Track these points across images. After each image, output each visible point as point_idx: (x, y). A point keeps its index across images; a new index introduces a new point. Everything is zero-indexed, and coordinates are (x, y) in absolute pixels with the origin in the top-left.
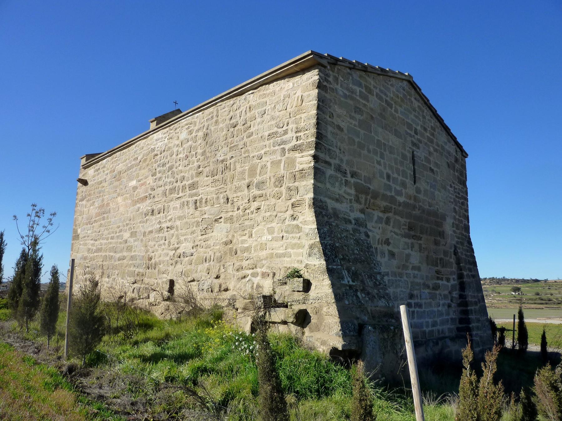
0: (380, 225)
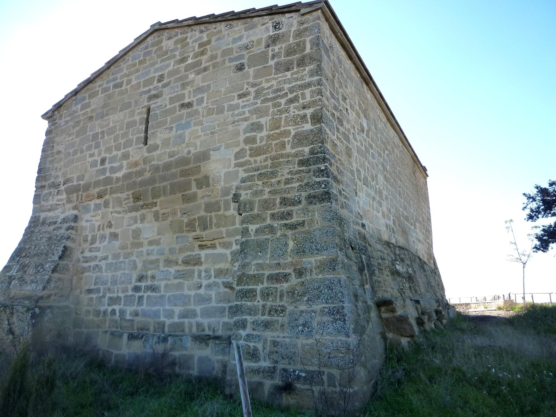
0: (100, 212)
